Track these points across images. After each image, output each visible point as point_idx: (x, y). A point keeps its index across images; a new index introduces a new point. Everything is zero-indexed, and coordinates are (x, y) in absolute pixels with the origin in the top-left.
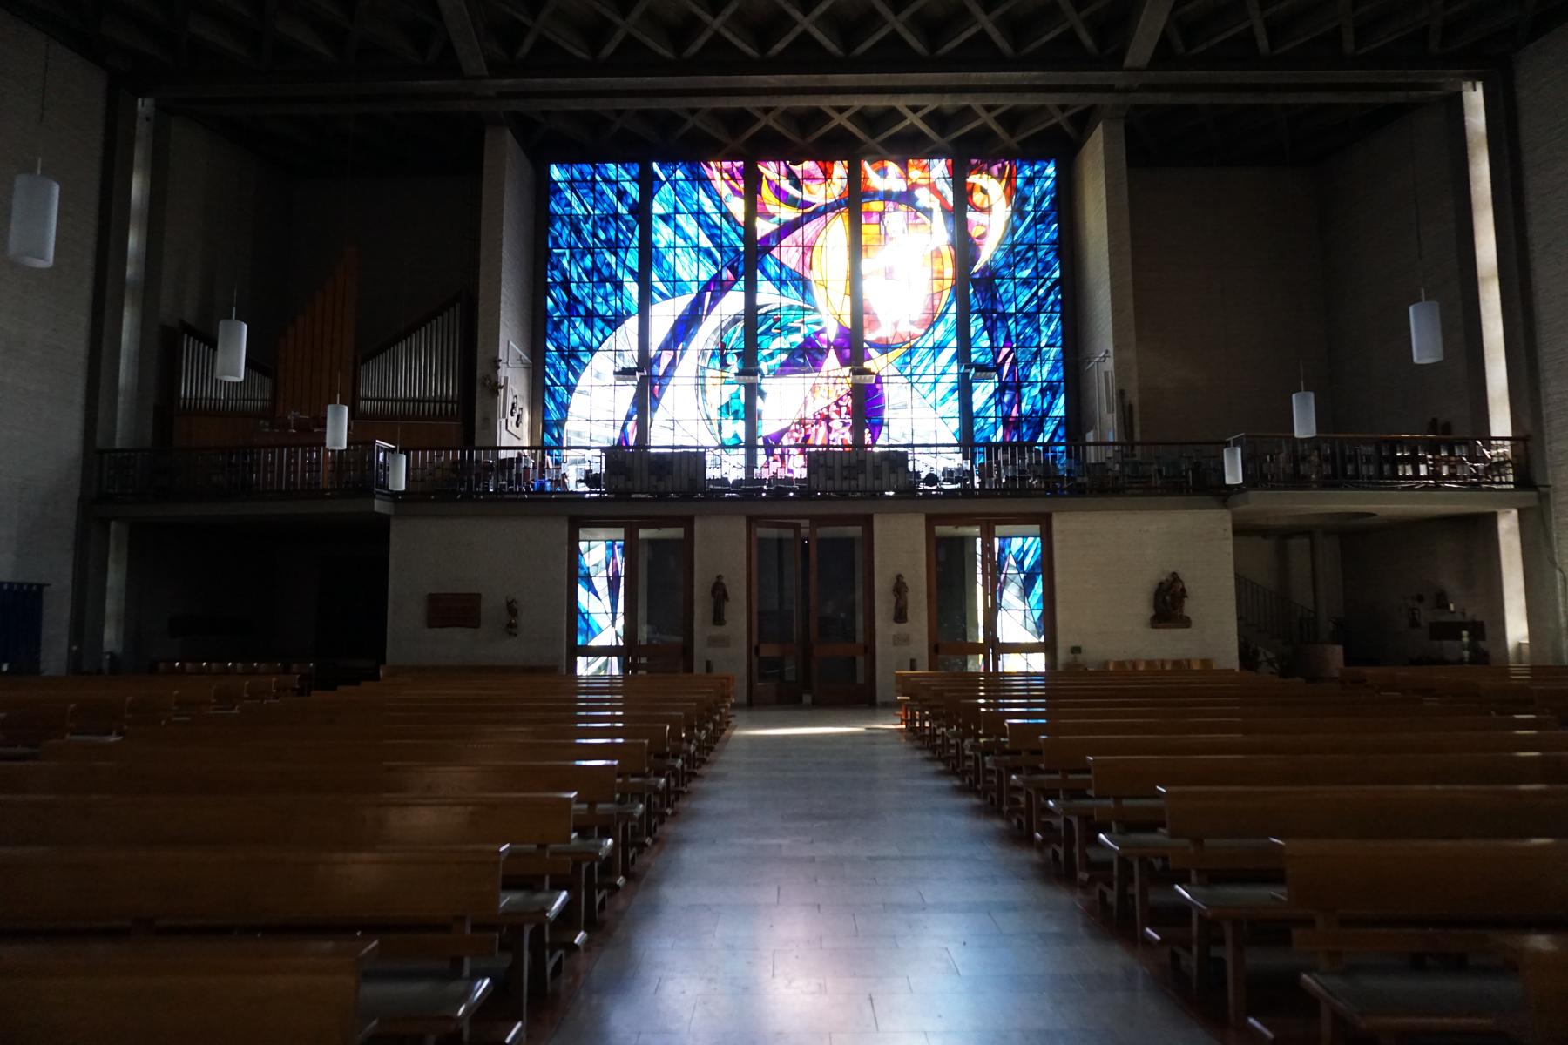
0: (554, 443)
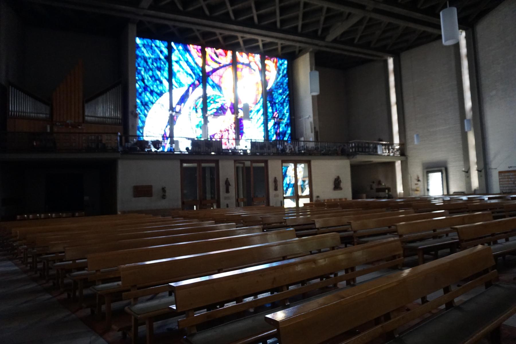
0: (140, 135)
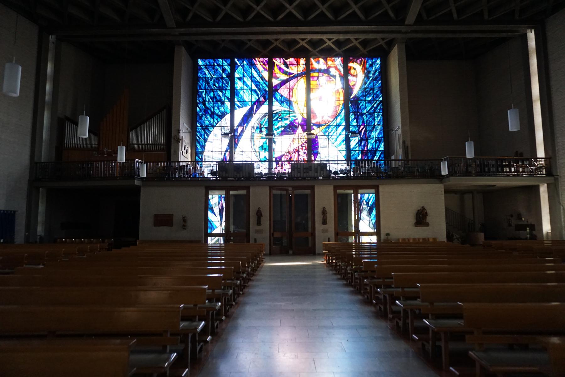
0: (199, 160)
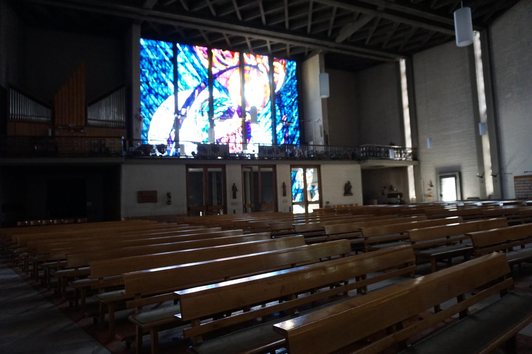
0: (145, 138)
